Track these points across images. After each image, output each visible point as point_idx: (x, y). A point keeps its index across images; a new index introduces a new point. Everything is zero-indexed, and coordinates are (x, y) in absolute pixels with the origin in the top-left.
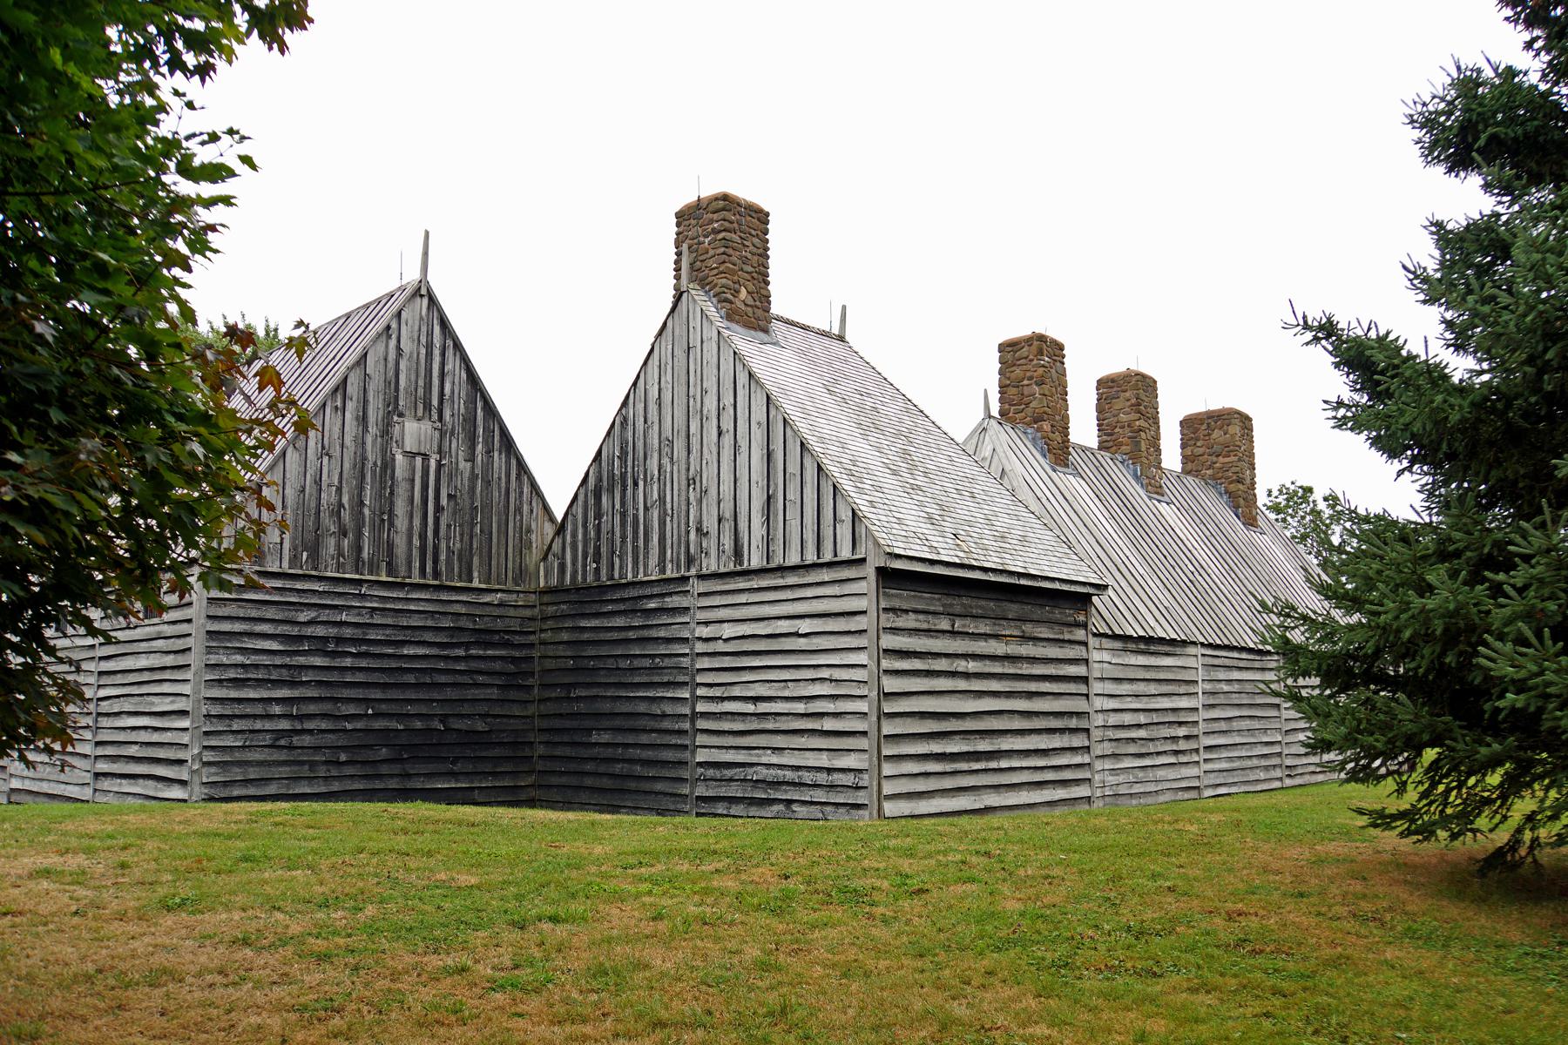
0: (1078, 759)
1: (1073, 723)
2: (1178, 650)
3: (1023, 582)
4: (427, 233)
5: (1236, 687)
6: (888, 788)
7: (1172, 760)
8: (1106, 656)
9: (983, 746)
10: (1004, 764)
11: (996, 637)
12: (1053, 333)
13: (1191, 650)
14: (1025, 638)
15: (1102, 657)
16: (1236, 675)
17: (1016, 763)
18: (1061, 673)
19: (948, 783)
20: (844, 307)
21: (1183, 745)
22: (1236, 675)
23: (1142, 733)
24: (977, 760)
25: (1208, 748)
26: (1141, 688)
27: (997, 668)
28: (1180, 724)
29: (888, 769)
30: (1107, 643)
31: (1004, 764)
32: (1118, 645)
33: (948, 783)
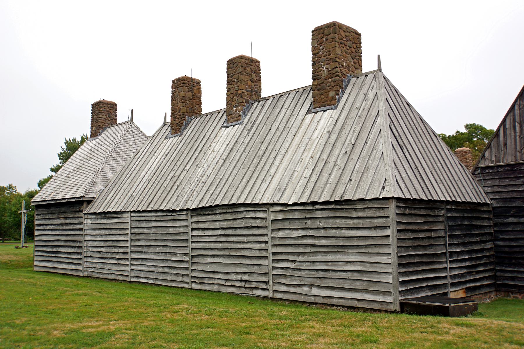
0: (79, 257)
1: (78, 244)
2: (119, 216)
3: (58, 202)
4: (379, 56)
5: (153, 230)
6: (35, 259)
7: (116, 262)
8: (89, 221)
9: (55, 250)
10: (59, 255)
11: (59, 218)
12: (195, 76)
13: (125, 215)
14: (66, 218)
15: (88, 221)
16: (154, 224)
17: (62, 256)
18: (74, 228)
19: (47, 259)
20: (132, 110)
21: (121, 256)
22: (154, 224)
23: (103, 250)
24: (54, 254)
25: (133, 259)
26: (103, 232)
27: (58, 227)
28: (120, 247)
29: (36, 254)
30: (90, 216)
31: (59, 255)
32: (94, 216)
33: (47, 259)
